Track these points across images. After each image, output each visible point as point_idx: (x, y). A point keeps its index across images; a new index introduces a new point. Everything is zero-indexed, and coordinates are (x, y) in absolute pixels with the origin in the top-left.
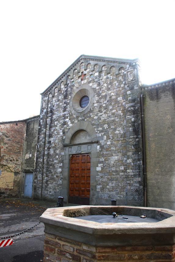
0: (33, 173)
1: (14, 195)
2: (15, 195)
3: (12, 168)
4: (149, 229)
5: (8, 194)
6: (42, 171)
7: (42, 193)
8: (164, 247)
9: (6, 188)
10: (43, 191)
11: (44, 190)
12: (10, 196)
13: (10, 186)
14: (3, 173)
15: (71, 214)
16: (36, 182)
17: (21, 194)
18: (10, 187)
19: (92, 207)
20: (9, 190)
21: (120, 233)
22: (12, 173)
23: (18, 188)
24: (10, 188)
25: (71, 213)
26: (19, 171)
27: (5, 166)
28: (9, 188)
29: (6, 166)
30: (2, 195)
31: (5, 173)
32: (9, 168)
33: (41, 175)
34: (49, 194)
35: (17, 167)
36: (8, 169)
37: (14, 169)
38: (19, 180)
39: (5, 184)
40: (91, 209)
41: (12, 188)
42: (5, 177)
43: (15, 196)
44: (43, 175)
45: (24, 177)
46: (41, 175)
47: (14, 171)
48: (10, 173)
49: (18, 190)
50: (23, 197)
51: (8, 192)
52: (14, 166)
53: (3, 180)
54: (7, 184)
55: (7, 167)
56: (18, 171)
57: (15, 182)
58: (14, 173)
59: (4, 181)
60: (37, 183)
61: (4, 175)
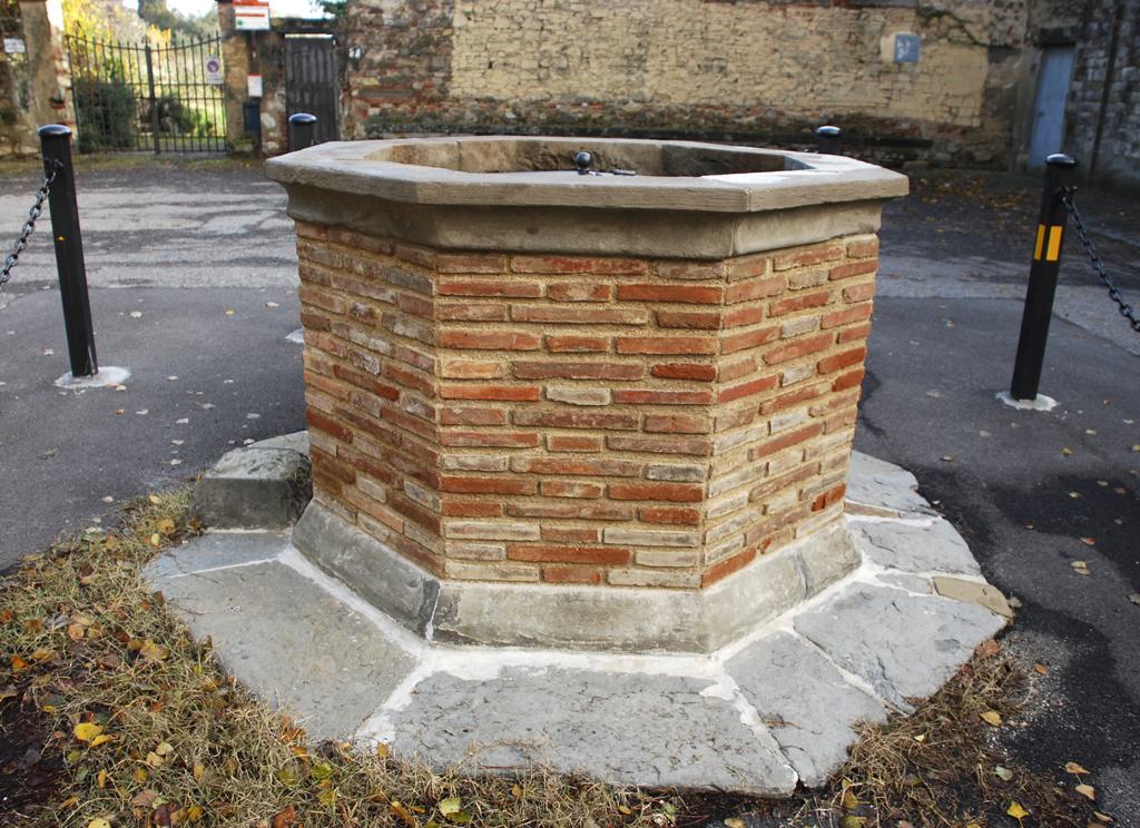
0: (1074, 44)
1: (981, 155)
2: (988, 157)
3: (979, 27)
4: (356, 176)
5: (954, 150)
6: (1110, 32)
7: (1101, 152)
8: (417, 254)
9: (941, 121)
10: (1103, 142)
11: (1110, 137)
12: (964, 160)
13: (962, 112)
14: (929, 49)
15: (556, 162)
16: (1079, 94)
17: (1018, 152)
18: (963, 117)
19: (669, 147)
20: (959, 130)
21: (304, 182)
22: (977, 48)
23: (1007, 122)
24: (966, 123)
25: (552, 157)
26: (1016, 41)
27: (940, 14)
28: (958, 122)
29: (946, 18)
30: (919, 152)
31: (942, 50)
32: (961, 25)
33: (1102, 53)
34: (1129, 159)
35: (1001, 19)
36: (955, 33)
37: (986, 28)
38: (1010, 86)
39: (939, 101)
40: (665, 152)
41: (976, 123)
42: (940, 71)
43: (991, 161)
44: (1112, 53)
45: (1033, 68)
46: (1102, 53)
47: (987, 42)
48: (965, 51)
49: (1007, 134)
50: (1024, 167)
51: (956, 142)
52: (986, 12)
53: (931, 83)
54: (950, 102)
55: (952, 22)
56: (1009, 41)
57: (989, 93)
58: (985, 50)
59: (936, 89)
60: (1083, 99)
61: (932, 63)
